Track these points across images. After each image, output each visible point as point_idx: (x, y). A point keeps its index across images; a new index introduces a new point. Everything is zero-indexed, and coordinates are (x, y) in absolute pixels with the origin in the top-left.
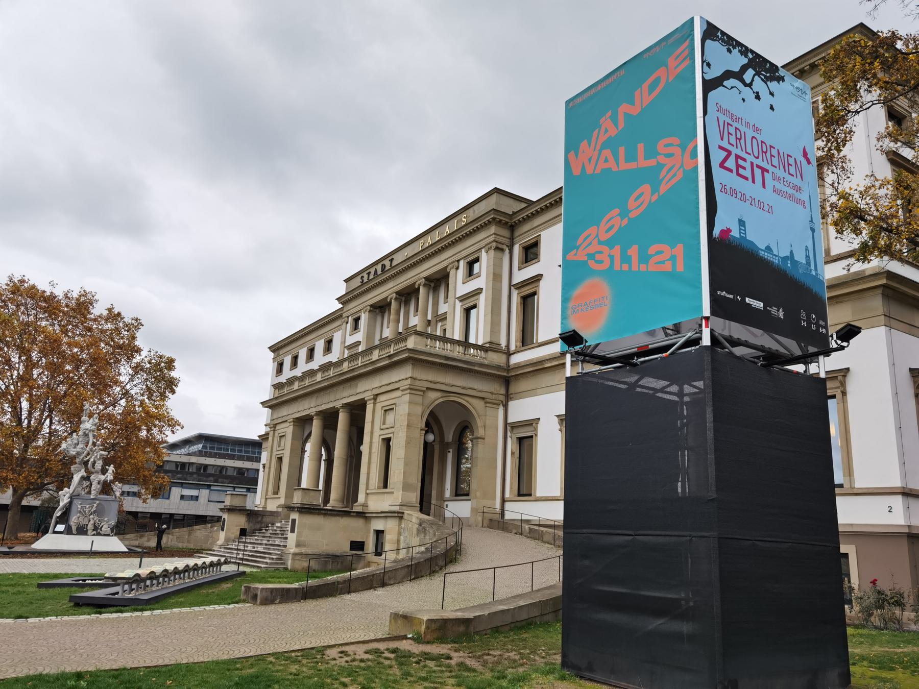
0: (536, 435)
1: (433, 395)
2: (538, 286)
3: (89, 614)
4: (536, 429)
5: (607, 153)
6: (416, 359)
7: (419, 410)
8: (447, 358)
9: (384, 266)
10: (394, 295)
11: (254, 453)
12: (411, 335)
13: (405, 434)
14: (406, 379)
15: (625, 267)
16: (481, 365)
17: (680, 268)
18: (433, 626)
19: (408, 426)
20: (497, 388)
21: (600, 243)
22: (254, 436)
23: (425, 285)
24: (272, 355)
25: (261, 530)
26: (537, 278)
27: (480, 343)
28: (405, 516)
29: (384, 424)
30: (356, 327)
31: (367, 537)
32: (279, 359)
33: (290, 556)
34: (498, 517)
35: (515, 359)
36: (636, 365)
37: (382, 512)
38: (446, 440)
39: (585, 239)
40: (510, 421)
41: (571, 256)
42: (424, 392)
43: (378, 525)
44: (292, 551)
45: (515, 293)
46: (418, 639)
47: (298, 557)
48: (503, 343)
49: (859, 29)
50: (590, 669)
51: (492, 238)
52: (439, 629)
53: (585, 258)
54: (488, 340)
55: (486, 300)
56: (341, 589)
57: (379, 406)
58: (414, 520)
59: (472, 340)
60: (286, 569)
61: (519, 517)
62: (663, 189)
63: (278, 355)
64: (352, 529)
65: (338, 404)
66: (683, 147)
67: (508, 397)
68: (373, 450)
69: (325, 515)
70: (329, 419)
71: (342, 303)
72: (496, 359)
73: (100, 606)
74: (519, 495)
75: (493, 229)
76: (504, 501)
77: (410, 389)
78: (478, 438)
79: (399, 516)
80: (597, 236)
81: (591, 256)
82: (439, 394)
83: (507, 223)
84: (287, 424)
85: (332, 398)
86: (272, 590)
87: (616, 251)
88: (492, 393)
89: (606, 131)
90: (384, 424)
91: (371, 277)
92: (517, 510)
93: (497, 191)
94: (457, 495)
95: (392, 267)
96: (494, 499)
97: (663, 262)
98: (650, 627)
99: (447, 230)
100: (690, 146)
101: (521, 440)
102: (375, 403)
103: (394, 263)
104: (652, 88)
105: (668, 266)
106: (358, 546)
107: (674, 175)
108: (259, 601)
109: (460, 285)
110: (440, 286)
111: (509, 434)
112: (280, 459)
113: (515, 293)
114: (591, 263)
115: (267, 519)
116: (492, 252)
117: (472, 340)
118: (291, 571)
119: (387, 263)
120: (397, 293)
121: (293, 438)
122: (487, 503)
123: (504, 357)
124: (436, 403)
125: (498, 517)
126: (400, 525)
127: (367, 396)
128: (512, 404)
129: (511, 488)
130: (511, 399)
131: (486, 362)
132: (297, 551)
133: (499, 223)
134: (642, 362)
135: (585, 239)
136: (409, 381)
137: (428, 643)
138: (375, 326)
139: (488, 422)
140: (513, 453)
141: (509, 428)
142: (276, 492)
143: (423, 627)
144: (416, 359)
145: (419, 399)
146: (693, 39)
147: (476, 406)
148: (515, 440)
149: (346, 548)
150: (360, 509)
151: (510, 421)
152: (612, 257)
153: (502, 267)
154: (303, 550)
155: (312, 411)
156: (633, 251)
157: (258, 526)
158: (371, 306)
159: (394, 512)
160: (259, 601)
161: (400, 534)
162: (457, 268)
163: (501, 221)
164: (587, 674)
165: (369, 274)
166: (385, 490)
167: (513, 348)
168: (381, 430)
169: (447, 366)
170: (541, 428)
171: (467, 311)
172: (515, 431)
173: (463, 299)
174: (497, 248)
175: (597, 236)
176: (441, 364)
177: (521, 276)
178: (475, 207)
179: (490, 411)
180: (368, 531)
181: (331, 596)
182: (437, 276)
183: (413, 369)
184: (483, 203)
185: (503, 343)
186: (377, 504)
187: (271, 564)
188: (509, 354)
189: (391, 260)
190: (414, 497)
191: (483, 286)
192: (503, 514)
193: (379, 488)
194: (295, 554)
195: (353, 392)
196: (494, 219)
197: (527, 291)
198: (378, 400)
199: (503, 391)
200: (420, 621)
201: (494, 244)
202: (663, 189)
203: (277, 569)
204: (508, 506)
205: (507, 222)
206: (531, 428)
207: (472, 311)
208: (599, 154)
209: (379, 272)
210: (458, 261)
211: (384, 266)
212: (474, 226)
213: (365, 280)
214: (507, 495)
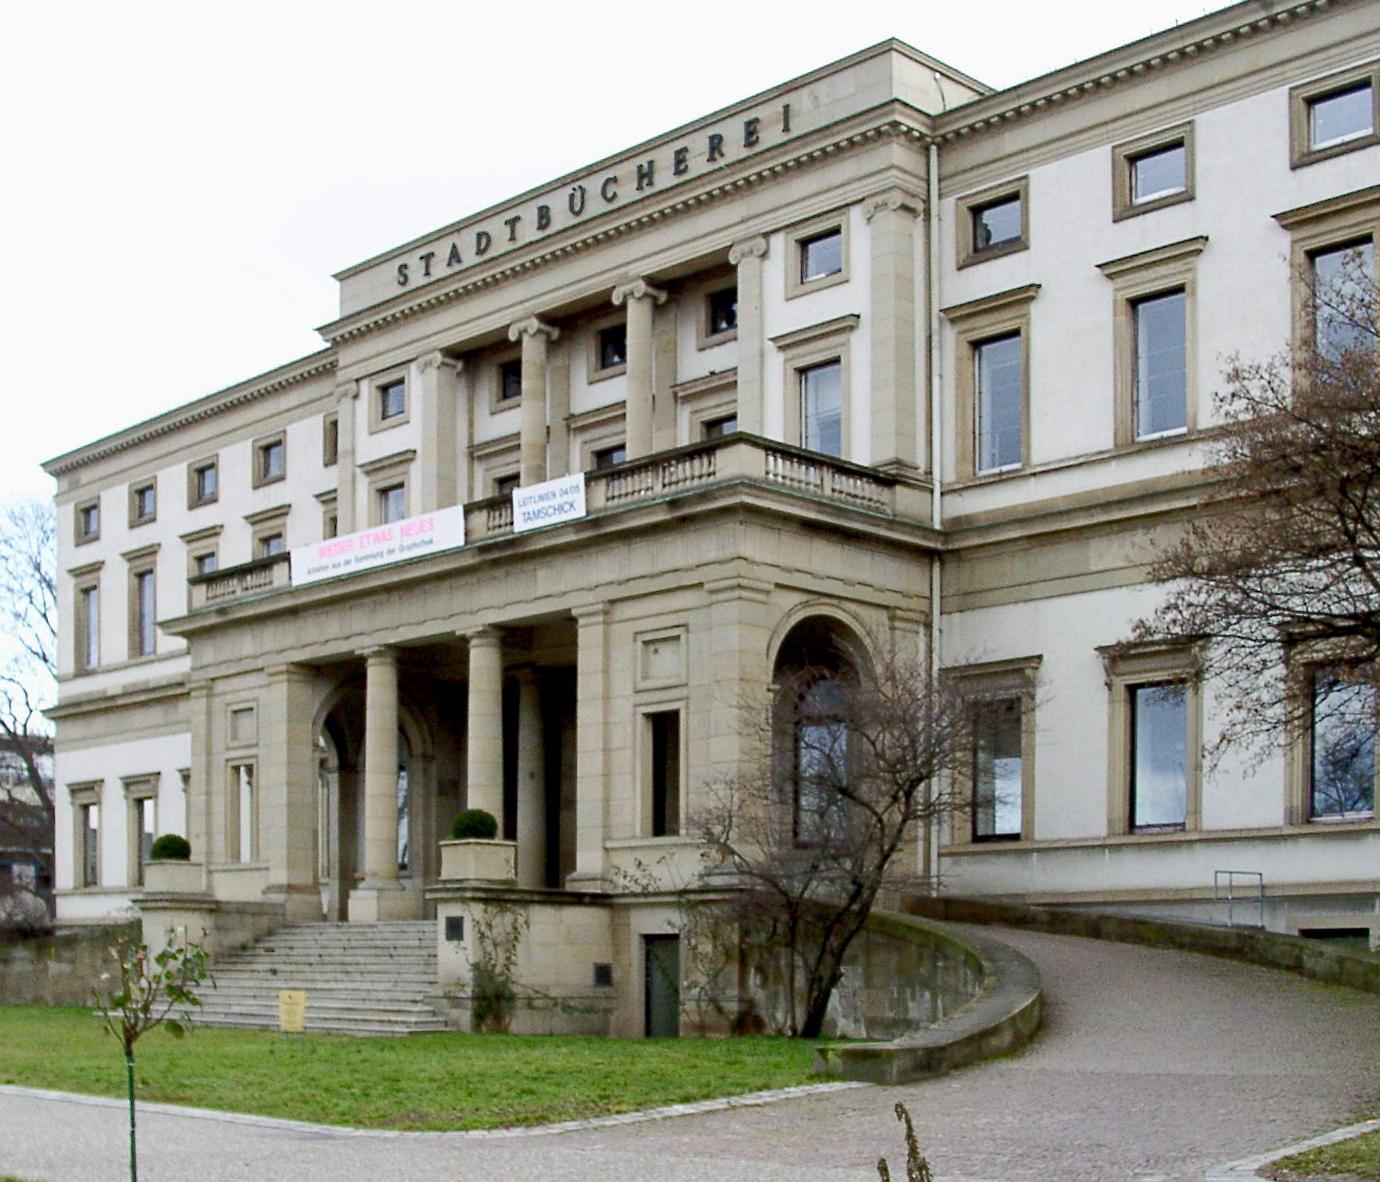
9: (484, 241)
26: (1023, 296)
32: (84, 496)
54: (889, 454)
63: (75, 486)
82: (796, 598)
91: (440, 270)
109: (772, 302)
165: (427, 258)
186: (628, 875)
211: (484, 241)
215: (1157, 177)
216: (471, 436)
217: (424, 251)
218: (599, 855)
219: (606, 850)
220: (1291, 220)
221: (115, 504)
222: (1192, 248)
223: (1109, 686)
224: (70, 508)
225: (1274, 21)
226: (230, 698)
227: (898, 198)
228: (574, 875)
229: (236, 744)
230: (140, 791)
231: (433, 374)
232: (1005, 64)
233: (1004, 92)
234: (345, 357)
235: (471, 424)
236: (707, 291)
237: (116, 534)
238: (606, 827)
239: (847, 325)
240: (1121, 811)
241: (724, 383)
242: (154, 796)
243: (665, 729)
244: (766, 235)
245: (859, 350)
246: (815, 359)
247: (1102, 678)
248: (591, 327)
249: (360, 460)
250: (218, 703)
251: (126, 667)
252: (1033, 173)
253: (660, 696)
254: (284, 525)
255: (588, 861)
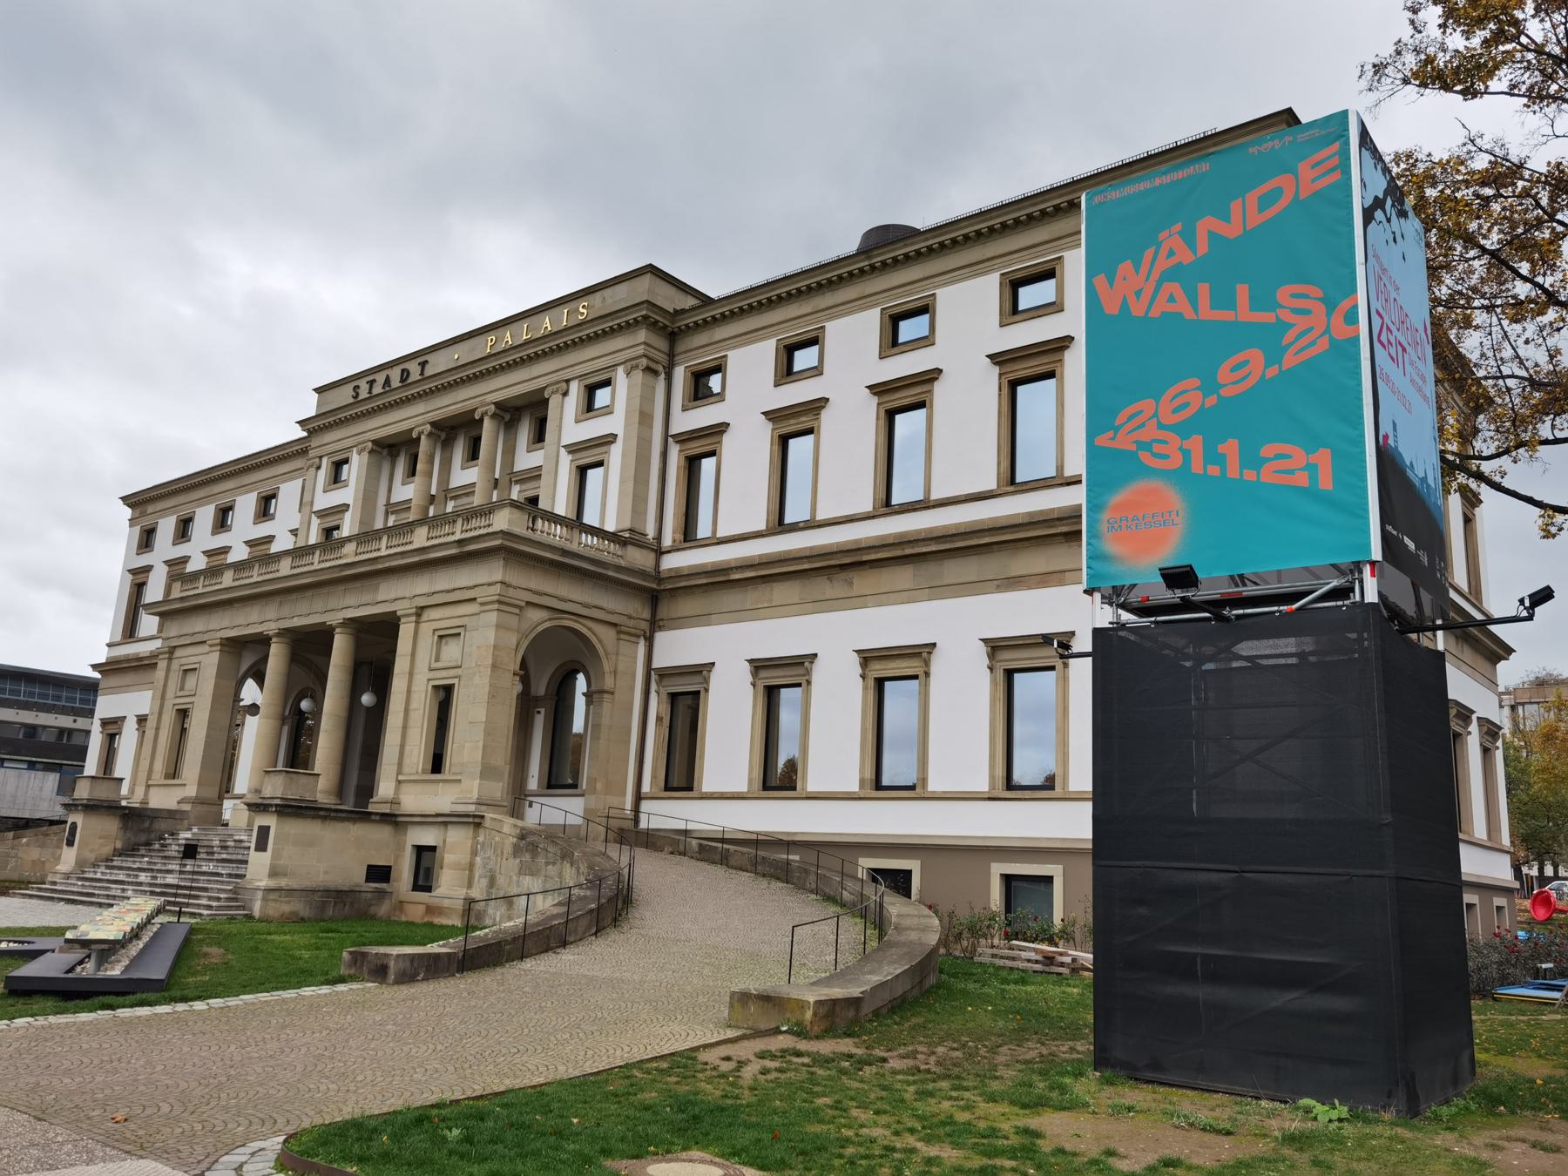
0: (707, 690)
1: (535, 615)
2: (720, 442)
3: (91, 1011)
4: (707, 681)
5: (1174, 287)
6: (510, 551)
7: (512, 639)
8: (565, 553)
9: (405, 374)
10: (428, 427)
11: (86, 701)
12: (504, 506)
13: (487, 681)
14: (490, 584)
15: (1214, 470)
16: (618, 568)
17: (1325, 483)
18: (822, 1011)
19: (494, 666)
20: (636, 609)
21: (1161, 426)
22: (80, 665)
23: (494, 416)
24: (127, 512)
25: (148, 844)
26: (720, 429)
27: (610, 527)
28: (487, 823)
29: (437, 660)
30: (336, 479)
31: (397, 858)
32: (147, 522)
33: (260, 894)
34: (629, 825)
35: (671, 562)
36: (1227, 619)
37: (438, 815)
38: (533, 693)
39: (1130, 418)
40: (655, 666)
41: (1103, 440)
42: (520, 608)
43: (427, 837)
44: (263, 884)
45: (675, 452)
46: (800, 1032)
47: (272, 896)
48: (651, 532)
49: (1285, 116)
50: (1156, 1066)
51: (640, 350)
52: (826, 1016)
53: (1133, 447)
54: (627, 525)
55: (624, 455)
56: (509, 953)
57: (426, 629)
58: (506, 829)
59: (590, 518)
60: (250, 917)
61: (681, 826)
62: (1289, 360)
63: (143, 514)
64: (371, 843)
65: (333, 619)
66: (1331, 305)
67: (655, 624)
68: (414, 705)
69: (324, 818)
70: (309, 647)
71: (308, 431)
72: (638, 558)
73: (69, 993)
74: (667, 788)
75: (642, 335)
76: (639, 797)
77: (499, 602)
78: (603, 692)
79: (476, 821)
80: (1155, 415)
81: (1143, 445)
82: (543, 614)
83: (665, 327)
84: (206, 648)
85: (319, 605)
86: (413, 957)
87: (1196, 443)
88: (630, 617)
89: (1171, 253)
90: (437, 660)
91: (377, 389)
92: (664, 814)
93: (651, 269)
94: (550, 786)
95: (424, 379)
96: (624, 794)
97: (1292, 472)
98: (1274, 1004)
99: (546, 323)
100: (1345, 304)
101: (674, 697)
102: (417, 623)
103: (429, 371)
104: (1265, 202)
105: (1302, 479)
106: (379, 874)
107: (1313, 343)
108: (392, 977)
109: (569, 425)
110: (519, 420)
111: (654, 687)
112: (183, 714)
113: (675, 452)
114: (1143, 455)
115: (162, 825)
116: (638, 376)
117: (590, 518)
118: (260, 920)
119: (413, 367)
120: (433, 424)
121: (219, 675)
122: (613, 801)
123: (652, 555)
124: (540, 628)
125: (629, 825)
126: (475, 837)
127: (401, 608)
128: (661, 638)
129: (654, 777)
130: (661, 628)
131: (623, 563)
132: (272, 883)
133: (653, 326)
134: (1238, 617)
135: (1130, 418)
136: (497, 589)
137: (817, 1038)
138: (378, 479)
139: (621, 667)
140: (659, 719)
141: (654, 677)
142: (173, 772)
143: (809, 1015)
144: (510, 551)
145: (513, 621)
146: (1347, 143)
147: (603, 637)
148: (664, 697)
149: (359, 875)
150: (386, 809)
151: (655, 666)
152: (1186, 453)
153: (653, 401)
154: (283, 882)
155: (270, 628)
156: (1230, 447)
157: (143, 838)
158: (375, 442)
159: (467, 816)
160: (392, 977)
161: (474, 853)
162: (565, 394)
163: (657, 322)
164: (1149, 1075)
165: (371, 383)
166: (437, 776)
167: (667, 542)
168: (431, 670)
169: (564, 566)
170: (716, 680)
171: (582, 471)
172: (666, 682)
173: (574, 449)
174: (648, 369)
175: (1155, 415)
176: (552, 563)
177: (686, 421)
178: (607, 292)
179: (624, 647)
180: (400, 848)
181: (495, 965)
182: (519, 403)
183: (505, 566)
184: (622, 289)
185: (651, 532)
186: (414, 801)
187: (219, 908)
188: (660, 552)
189: (423, 364)
190: (498, 789)
191: (618, 429)
192: (636, 820)
193: (424, 772)
194: (268, 890)
195: (366, 598)
196: (645, 317)
197: (696, 448)
198: (425, 617)
199: (646, 614)
200: (802, 1005)
201: (644, 362)
202: (1289, 360)
203: (232, 918)
204: (645, 806)
205: (667, 326)
206: (698, 679)
207: (590, 473)
208: (1157, 289)
209: (396, 383)
210: (568, 381)
211: (405, 374)
212: (606, 326)
213: (363, 394)
214: (646, 788)
215: (910, 329)
216: (389, 498)
217: (370, 378)
218: (393, 785)
219: (399, 782)
220: (878, 390)
221: (167, 527)
222: (932, 376)
223: (754, 685)
224: (138, 529)
225: (873, 268)
226: (183, 661)
227: (644, 362)
228: (374, 799)
229: (439, 665)
230: (774, 677)
231: (365, 456)
232: (717, 280)
233: (720, 300)
234: (315, 442)
235: (390, 491)
236: (529, 413)
237: (165, 546)
238: (400, 764)
239: (610, 439)
240: (869, 774)
241: (534, 475)
242: (802, 683)
243: (444, 697)
244: (568, 381)
245: (615, 454)
246: (588, 458)
247: (751, 679)
248: (458, 431)
249: (564, 443)
250: (175, 665)
251: (873, 517)
252: (1066, 254)
253: (444, 674)
254: (930, 392)
255: (385, 788)
